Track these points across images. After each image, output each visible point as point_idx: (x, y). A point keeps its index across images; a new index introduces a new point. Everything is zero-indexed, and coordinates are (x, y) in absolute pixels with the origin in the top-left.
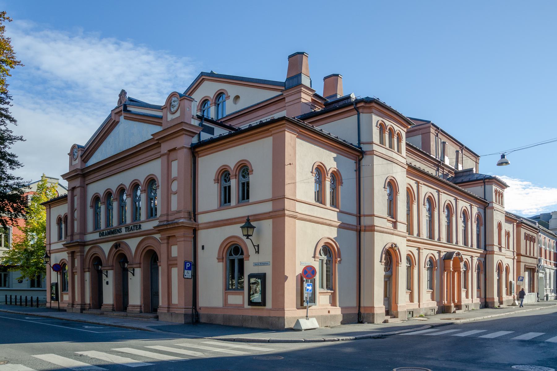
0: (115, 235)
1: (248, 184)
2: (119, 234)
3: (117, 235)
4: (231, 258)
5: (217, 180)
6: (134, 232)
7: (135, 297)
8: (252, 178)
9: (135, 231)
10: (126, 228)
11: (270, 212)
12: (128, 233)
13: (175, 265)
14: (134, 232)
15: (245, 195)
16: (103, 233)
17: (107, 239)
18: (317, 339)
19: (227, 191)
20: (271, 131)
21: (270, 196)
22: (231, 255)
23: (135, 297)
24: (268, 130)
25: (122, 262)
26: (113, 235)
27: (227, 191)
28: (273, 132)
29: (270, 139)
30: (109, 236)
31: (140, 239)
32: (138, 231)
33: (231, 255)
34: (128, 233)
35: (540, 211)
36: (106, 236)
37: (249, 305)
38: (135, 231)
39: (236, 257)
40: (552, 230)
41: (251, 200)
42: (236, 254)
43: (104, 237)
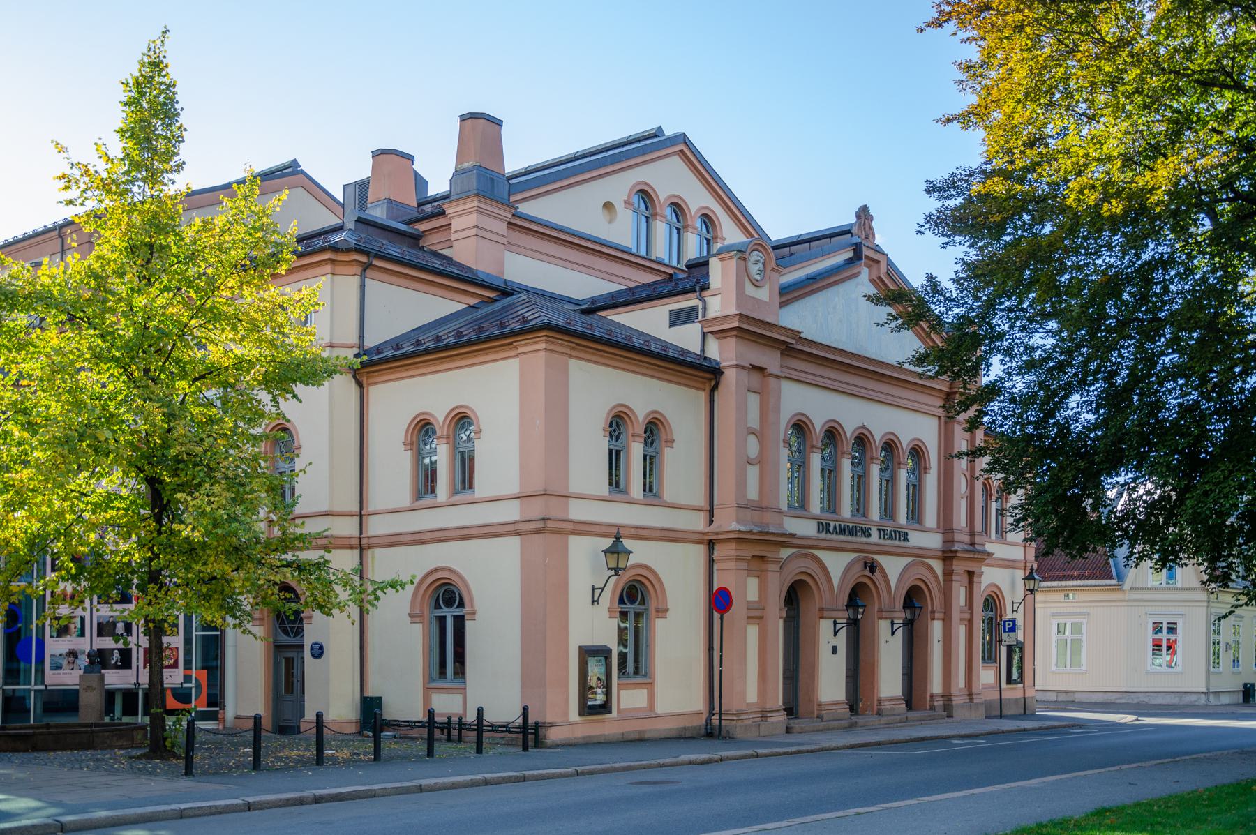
0: (853, 539)
2: (864, 539)
3: (858, 539)
4: (439, 613)
5: (409, 444)
7: (889, 681)
11: (516, 522)
12: (882, 541)
13: (750, 606)
17: (843, 545)
18: (967, 732)
20: (516, 348)
21: (515, 489)
22: (621, 601)
23: (889, 681)
24: (511, 344)
26: (850, 538)
28: (521, 350)
29: (515, 362)
30: (842, 537)
31: (910, 559)
33: (437, 606)
34: (882, 541)
36: (834, 537)
37: (580, 715)
38: (897, 543)
39: (449, 613)
41: (481, 490)
42: (633, 601)
43: (829, 536)
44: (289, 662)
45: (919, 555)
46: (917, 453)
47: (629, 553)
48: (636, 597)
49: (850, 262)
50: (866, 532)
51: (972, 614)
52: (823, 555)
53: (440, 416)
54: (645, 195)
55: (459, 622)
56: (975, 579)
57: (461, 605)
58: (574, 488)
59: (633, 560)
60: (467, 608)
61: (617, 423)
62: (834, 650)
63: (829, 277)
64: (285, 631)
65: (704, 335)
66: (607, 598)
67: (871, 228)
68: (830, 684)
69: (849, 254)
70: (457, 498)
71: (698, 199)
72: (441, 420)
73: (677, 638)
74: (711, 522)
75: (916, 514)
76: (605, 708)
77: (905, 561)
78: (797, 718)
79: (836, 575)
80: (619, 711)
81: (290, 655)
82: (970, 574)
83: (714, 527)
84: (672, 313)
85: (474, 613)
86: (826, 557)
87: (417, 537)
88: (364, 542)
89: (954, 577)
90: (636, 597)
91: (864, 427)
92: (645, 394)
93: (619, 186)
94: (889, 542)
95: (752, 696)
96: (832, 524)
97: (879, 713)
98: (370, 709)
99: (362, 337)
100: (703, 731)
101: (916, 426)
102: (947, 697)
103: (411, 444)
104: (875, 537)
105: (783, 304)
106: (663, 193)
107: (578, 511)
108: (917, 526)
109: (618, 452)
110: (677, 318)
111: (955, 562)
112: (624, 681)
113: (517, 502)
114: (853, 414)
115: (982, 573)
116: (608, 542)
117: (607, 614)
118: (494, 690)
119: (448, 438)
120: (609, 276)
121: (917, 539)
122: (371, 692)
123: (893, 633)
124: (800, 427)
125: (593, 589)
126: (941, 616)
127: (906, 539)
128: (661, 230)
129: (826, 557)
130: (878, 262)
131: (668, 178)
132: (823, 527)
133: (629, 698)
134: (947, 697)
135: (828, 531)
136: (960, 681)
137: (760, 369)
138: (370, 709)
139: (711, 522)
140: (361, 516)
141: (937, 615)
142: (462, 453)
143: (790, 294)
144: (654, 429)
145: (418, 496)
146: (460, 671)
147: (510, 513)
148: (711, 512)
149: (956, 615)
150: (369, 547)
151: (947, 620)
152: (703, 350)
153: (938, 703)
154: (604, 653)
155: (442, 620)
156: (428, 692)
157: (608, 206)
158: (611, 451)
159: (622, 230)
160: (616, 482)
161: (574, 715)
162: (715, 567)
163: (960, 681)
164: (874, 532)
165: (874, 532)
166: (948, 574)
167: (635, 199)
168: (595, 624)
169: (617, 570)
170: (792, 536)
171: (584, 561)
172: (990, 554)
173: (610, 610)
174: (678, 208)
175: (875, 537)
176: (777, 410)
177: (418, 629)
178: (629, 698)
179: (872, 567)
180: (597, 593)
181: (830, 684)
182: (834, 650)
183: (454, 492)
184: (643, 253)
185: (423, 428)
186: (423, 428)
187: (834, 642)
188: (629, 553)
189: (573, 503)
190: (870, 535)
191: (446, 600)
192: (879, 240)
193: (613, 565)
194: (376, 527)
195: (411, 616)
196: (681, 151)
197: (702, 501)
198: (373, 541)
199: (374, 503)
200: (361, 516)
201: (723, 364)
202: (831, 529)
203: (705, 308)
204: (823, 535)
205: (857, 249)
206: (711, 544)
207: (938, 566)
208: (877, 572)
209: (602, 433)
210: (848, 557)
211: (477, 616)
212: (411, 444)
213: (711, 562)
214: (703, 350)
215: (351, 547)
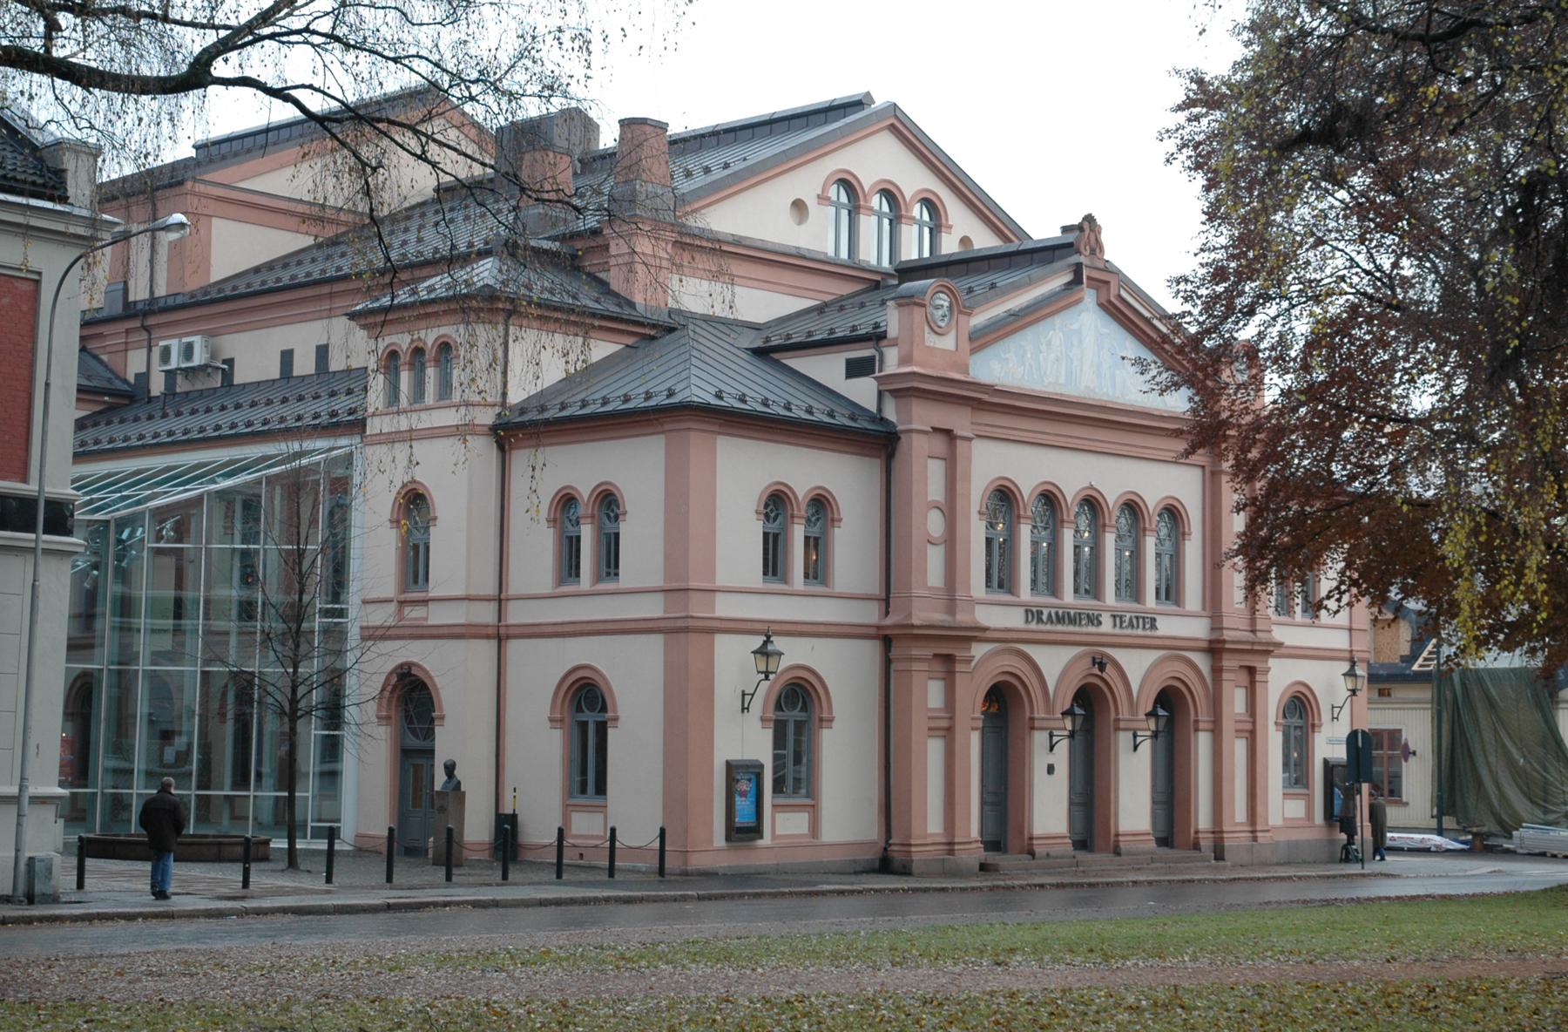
0: (1077, 629)
1: (617, 535)
2: (1092, 629)
3: (1084, 629)
4: (781, 715)
5: (553, 521)
6: (1135, 632)
7: (1133, 807)
8: (626, 530)
9: (1140, 632)
10: (1114, 617)
12: (1118, 631)
14: (1135, 632)
15: (610, 561)
16: (1040, 613)
19: (571, 546)
21: (658, 581)
22: (778, 707)
23: (1133, 807)
25: (1091, 704)
26: (1071, 628)
27: (571, 546)
28: (666, 427)
30: (1060, 628)
31: (1161, 653)
32: (1148, 633)
34: (1118, 631)
35: (352, 709)
36: (1049, 627)
39: (591, 717)
40: (922, 875)
43: (1042, 627)
44: (417, 768)
45: (1174, 647)
46: (1173, 513)
47: (780, 654)
48: (797, 702)
49: (1069, 285)
50: (1094, 620)
51: (1254, 723)
52: (1033, 651)
53: (585, 490)
54: (847, 184)
55: (602, 730)
56: (1258, 678)
57: (604, 709)
58: (721, 580)
59: (785, 662)
60: (610, 714)
61: (776, 502)
62: (1051, 769)
63: (1040, 308)
64: (414, 732)
65: (880, 394)
66: (757, 706)
67: (1098, 241)
68: (1049, 809)
69: (1068, 277)
70: (601, 587)
71: (913, 179)
72: (586, 497)
73: (843, 753)
74: (887, 613)
75: (1171, 591)
76: (756, 831)
77: (1152, 656)
78: (1006, 852)
79: (1051, 675)
80: (774, 836)
81: (419, 761)
82: (1251, 671)
83: (889, 621)
84: (849, 363)
85: (616, 719)
86: (1038, 653)
87: (559, 629)
88: (503, 631)
89: (1225, 676)
90: (797, 702)
91: (1091, 487)
92: (807, 470)
93: (809, 181)
94: (1129, 631)
95: (934, 825)
96: (1046, 612)
97: (1117, 852)
98: (507, 828)
99: (504, 394)
100: (877, 865)
101: (1171, 481)
102: (1217, 833)
103: (555, 520)
104: (1107, 626)
105: (973, 351)
106: (868, 178)
107: (726, 607)
108: (1170, 607)
109: (776, 536)
110: (856, 369)
111: (1225, 656)
112: (781, 801)
113: (660, 596)
114: (1073, 473)
115: (1267, 671)
116: (758, 641)
117: (759, 724)
118: (634, 808)
119: (593, 516)
120: (795, 291)
121: (1169, 627)
122: (507, 809)
123: (1136, 748)
124: (1004, 496)
125: (744, 695)
126: (1210, 726)
127: (1153, 627)
128: (867, 224)
129: (1038, 653)
130: (1107, 283)
131: (876, 161)
132: (1033, 614)
133: (784, 825)
134: (1217, 833)
135: (1040, 620)
136: (1238, 811)
137: (948, 433)
138: (507, 828)
139: (887, 613)
140: (500, 600)
141: (1201, 726)
142: (608, 535)
143: (982, 339)
144: (821, 504)
145: (560, 581)
146: (601, 789)
147: (652, 608)
148: (887, 601)
149: (1228, 727)
150: (508, 637)
151: (1216, 730)
152: (880, 409)
153: (1206, 843)
154: (755, 770)
155: (583, 726)
156: (567, 810)
157: (799, 206)
158: (766, 535)
159: (820, 235)
160: (773, 563)
161: (719, 840)
162: (893, 667)
163: (1238, 811)
164: (1106, 620)
165: (1106, 620)
166: (1217, 671)
167: (832, 192)
168: (746, 738)
169: (767, 674)
170: (986, 629)
171: (732, 659)
172: (1280, 645)
173: (763, 720)
174: (890, 194)
175: (1107, 626)
176: (968, 478)
177: (557, 735)
178: (784, 825)
179: (1100, 663)
180: (748, 698)
181: (1049, 809)
182: (1051, 769)
183: (598, 578)
184: (844, 255)
185: (567, 500)
186: (567, 500)
187: (1051, 759)
188: (780, 654)
189: (720, 599)
190: (1100, 623)
191: (586, 700)
192: (1108, 255)
193: (762, 668)
194: (517, 614)
195: (552, 720)
196: (892, 125)
197: (874, 586)
198: (512, 631)
199: (514, 587)
200: (500, 600)
201: (900, 428)
202: (1045, 617)
203: (882, 361)
204: (1033, 626)
205: (1078, 269)
206: (887, 641)
207: (1202, 661)
208: (1109, 668)
209: (755, 516)
210: (1067, 654)
211: (620, 724)
212: (555, 520)
213: (887, 662)
214: (880, 409)
215: (488, 637)
